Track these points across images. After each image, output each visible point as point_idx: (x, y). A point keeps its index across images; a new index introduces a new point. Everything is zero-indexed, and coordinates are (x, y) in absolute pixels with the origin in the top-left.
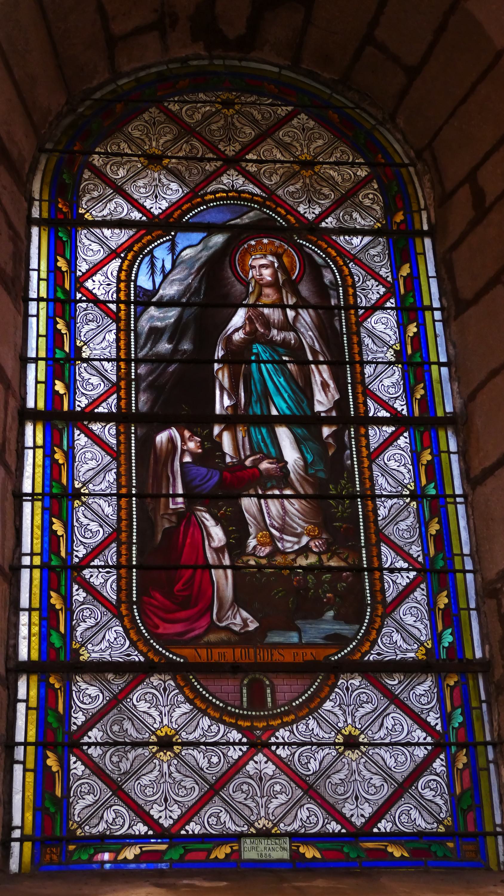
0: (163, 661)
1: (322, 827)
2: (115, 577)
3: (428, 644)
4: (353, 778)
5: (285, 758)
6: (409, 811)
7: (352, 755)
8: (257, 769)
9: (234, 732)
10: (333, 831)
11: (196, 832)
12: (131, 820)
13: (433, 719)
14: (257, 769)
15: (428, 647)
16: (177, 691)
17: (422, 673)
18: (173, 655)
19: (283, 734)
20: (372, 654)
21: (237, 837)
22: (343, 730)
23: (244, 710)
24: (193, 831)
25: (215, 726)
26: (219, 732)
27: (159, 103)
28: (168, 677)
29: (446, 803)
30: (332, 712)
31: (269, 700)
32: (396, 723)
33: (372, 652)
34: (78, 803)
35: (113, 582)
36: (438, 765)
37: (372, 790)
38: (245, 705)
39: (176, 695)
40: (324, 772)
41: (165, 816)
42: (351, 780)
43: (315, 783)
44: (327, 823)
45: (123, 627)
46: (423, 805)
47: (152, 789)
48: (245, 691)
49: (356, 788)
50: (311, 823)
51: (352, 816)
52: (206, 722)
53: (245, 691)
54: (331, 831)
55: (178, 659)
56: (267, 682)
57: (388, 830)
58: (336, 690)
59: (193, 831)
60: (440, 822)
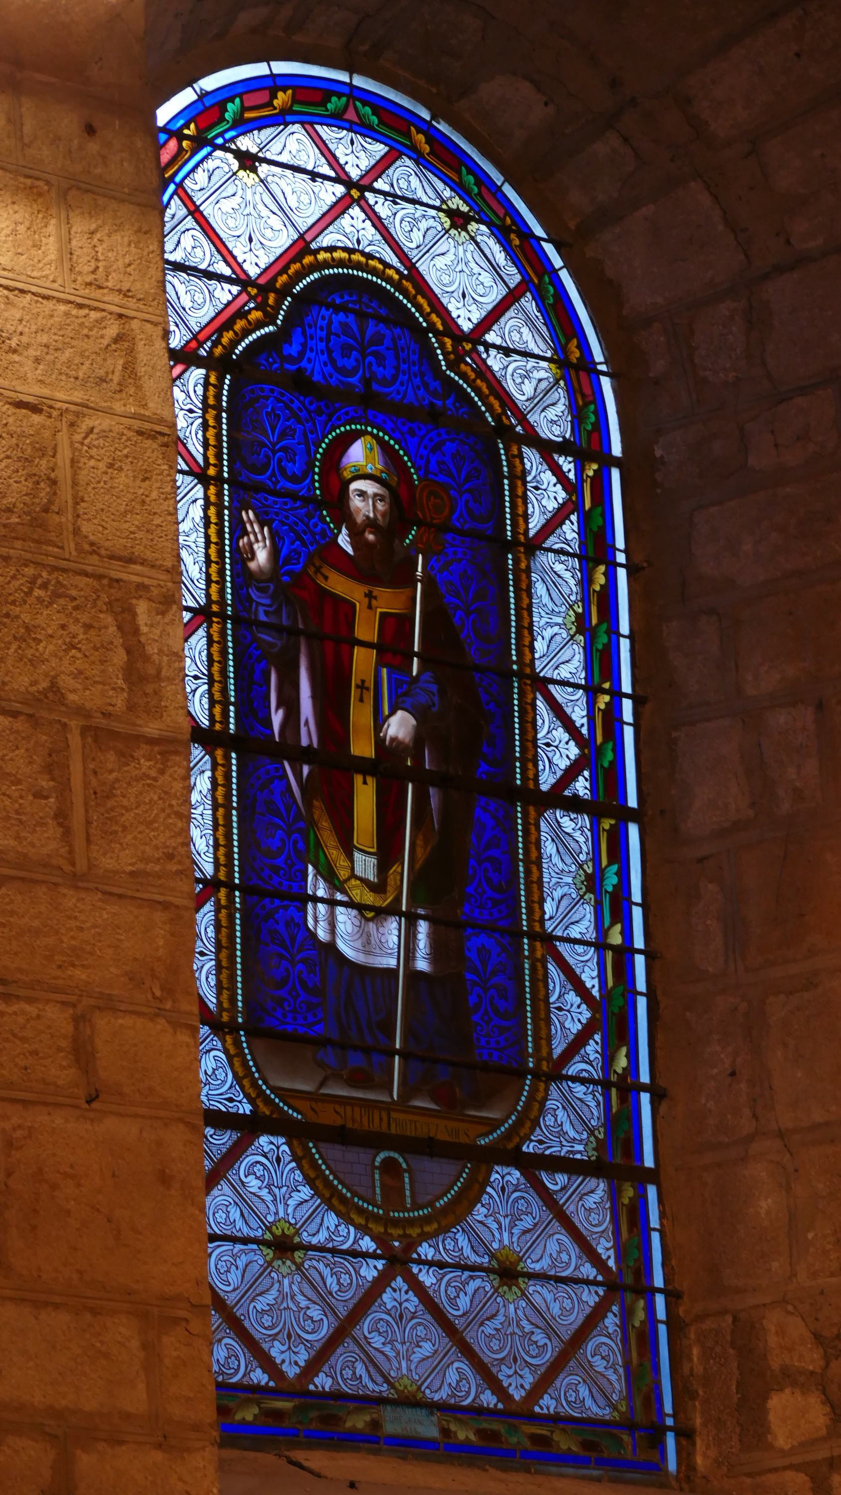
0: (274, 1116)
1: (244, 1375)
2: (213, 963)
3: (600, 1133)
4: (285, 1305)
5: (429, 1288)
6: (354, 1363)
7: (286, 1267)
8: (395, 1300)
9: (367, 1238)
10: (259, 1382)
11: (327, 1389)
12: (477, 1386)
13: (605, 1248)
14: (395, 1300)
15: (600, 1137)
16: (293, 1164)
17: (224, 1128)
18: (289, 1107)
19: (426, 1250)
20: (532, 1141)
21: (379, 1401)
22: (274, 1227)
23: (408, 1211)
24: (323, 1388)
25: (343, 1226)
26: (347, 1237)
27: (308, 124)
28: (282, 1140)
29: (619, 1380)
30: (259, 1197)
31: (408, 1193)
32: (554, 1251)
33: (532, 1138)
34: (414, 1353)
35: (208, 973)
36: (611, 1322)
37: (534, 1351)
38: (379, 1198)
39: (292, 1170)
40: (479, 1315)
41: (291, 1361)
42: (282, 1307)
43: (562, 1340)
44: (251, 1371)
45: (226, 1052)
46: (592, 1379)
47: (419, 1334)
48: (377, 1176)
49: (288, 1321)
50: (230, 1368)
51: (283, 1361)
52: (331, 1219)
53: (377, 1176)
54: (485, 1405)
55: (295, 1115)
56: (404, 1166)
57: (491, 1406)
58: (489, 1189)
59: (488, 1404)
60: (614, 1408)
